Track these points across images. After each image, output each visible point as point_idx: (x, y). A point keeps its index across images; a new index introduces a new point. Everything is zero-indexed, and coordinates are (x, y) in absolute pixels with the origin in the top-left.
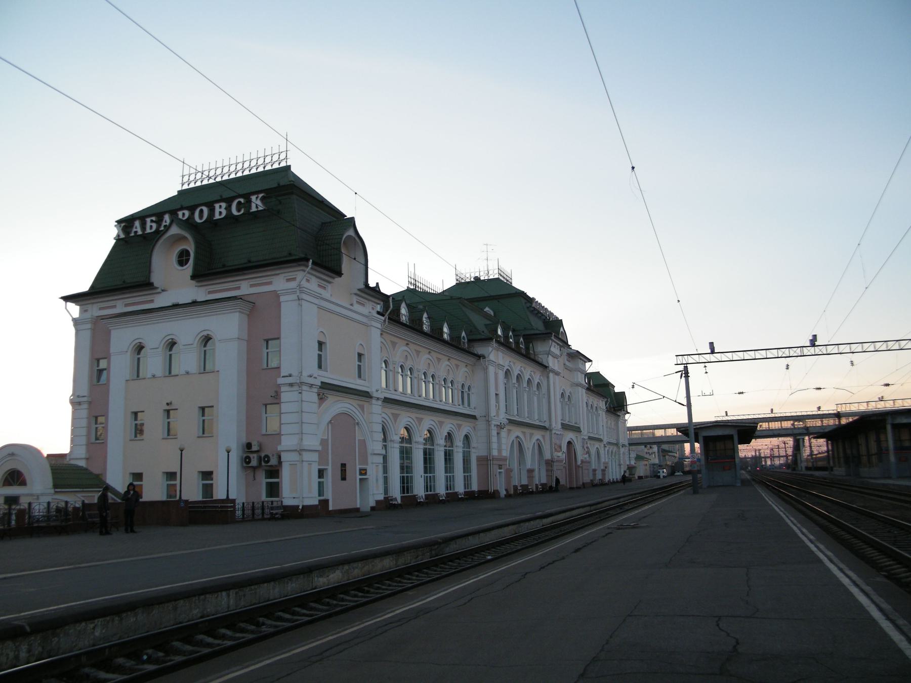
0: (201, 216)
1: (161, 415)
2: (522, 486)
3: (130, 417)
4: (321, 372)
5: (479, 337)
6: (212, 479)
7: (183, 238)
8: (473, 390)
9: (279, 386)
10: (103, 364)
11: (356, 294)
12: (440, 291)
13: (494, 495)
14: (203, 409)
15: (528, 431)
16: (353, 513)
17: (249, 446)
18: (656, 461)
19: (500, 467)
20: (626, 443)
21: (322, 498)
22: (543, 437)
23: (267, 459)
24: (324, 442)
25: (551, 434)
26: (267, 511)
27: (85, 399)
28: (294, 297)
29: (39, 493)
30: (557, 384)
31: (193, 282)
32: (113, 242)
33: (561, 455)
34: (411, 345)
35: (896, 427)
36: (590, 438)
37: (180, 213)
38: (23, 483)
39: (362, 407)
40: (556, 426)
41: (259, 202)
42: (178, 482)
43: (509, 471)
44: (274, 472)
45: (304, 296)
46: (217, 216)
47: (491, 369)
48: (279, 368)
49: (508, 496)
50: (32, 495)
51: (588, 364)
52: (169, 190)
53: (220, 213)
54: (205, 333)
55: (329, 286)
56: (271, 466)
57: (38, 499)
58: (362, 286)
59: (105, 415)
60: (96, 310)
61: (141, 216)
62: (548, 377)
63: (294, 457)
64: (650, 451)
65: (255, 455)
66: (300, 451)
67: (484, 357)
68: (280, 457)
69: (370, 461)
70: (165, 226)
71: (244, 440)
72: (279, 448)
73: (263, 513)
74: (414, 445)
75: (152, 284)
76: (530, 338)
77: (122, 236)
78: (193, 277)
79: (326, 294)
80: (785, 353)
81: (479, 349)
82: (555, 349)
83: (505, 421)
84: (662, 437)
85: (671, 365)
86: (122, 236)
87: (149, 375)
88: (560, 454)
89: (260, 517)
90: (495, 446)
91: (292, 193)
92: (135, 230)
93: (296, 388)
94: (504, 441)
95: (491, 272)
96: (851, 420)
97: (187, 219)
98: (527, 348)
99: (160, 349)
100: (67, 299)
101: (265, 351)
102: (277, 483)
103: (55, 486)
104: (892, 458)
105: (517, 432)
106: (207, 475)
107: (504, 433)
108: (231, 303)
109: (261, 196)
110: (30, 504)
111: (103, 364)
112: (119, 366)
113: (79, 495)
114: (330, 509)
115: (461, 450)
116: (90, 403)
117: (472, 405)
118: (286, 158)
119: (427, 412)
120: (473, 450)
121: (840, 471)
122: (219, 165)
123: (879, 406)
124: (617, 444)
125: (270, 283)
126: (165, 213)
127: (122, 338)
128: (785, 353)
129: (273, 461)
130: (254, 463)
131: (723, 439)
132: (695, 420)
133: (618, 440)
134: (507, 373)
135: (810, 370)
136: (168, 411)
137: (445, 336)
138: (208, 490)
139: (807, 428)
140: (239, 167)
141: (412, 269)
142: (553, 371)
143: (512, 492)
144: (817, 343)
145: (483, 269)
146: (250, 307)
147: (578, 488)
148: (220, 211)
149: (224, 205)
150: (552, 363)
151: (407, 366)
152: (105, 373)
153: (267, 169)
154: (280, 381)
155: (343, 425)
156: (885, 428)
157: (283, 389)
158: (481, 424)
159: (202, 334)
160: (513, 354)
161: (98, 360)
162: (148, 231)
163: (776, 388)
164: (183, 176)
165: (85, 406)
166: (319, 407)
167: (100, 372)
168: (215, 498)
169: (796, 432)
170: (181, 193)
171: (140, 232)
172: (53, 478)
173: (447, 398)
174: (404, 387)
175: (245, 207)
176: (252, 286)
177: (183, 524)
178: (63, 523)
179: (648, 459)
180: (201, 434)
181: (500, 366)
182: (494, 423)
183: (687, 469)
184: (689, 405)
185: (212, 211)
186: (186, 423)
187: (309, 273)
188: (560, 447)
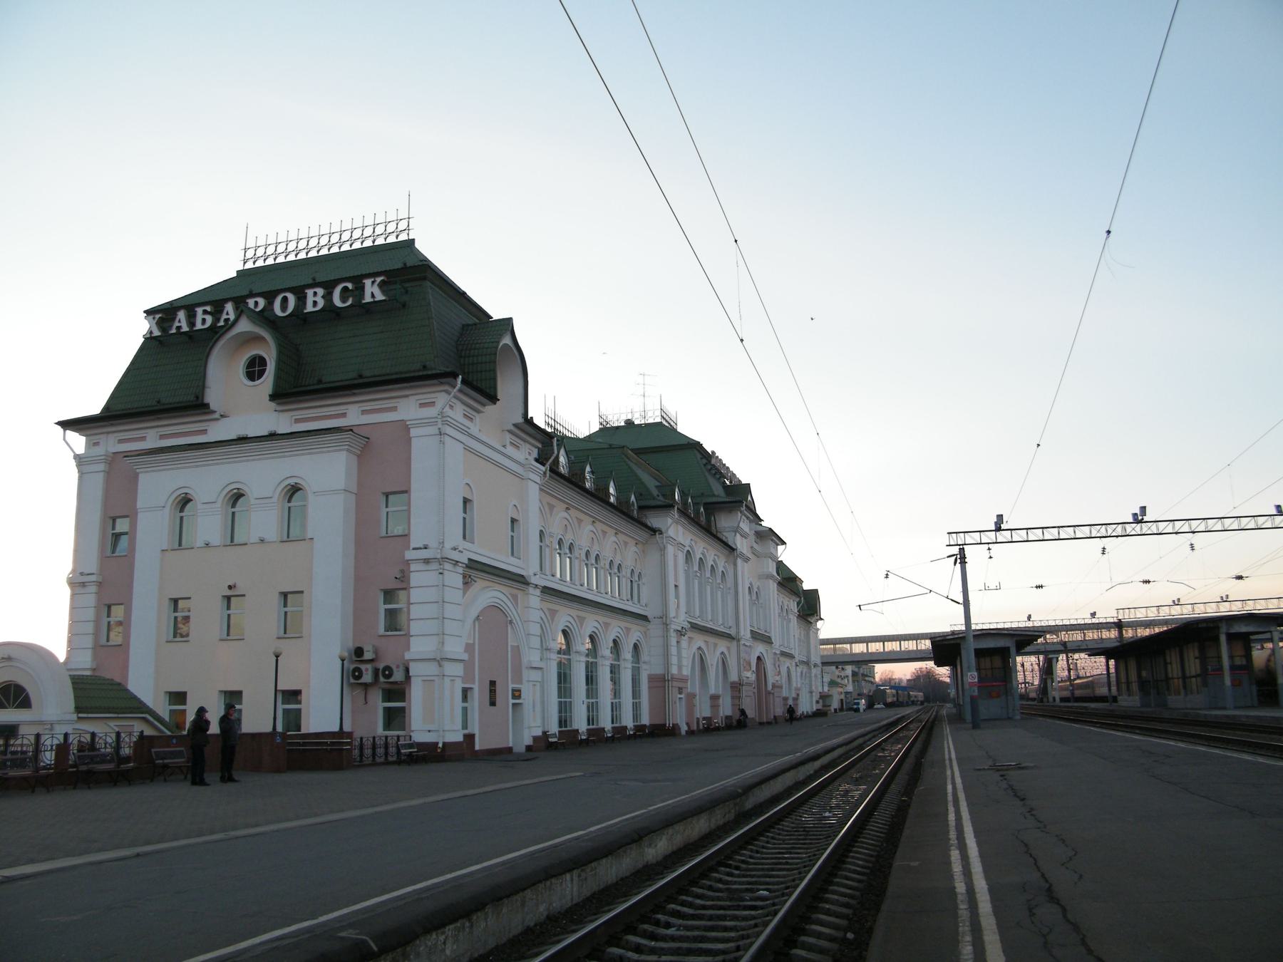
0: (284, 308)
1: (219, 604)
2: (704, 719)
3: (167, 606)
4: (467, 545)
5: (653, 503)
6: (300, 703)
7: (257, 339)
8: (644, 580)
9: (408, 563)
10: (122, 526)
11: (510, 431)
12: (581, 436)
13: (672, 732)
14: (285, 595)
15: (712, 640)
16: (503, 754)
17: (359, 652)
18: (850, 688)
19: (680, 690)
20: (819, 661)
21: (466, 732)
22: (728, 648)
23: (388, 671)
24: (469, 648)
25: (738, 646)
26: (392, 750)
27: (93, 578)
28: (433, 430)
29: (51, 718)
30: (746, 573)
31: (273, 405)
33: (750, 676)
34: (572, 511)
35: (1231, 637)
36: (784, 654)
37: (251, 302)
39: (515, 597)
40: (745, 634)
42: (280, 707)
43: (691, 696)
44: (397, 692)
45: (449, 430)
46: (310, 308)
47: (670, 550)
48: (406, 536)
49: (691, 733)
50: (41, 723)
51: (781, 548)
52: (227, 271)
53: (315, 303)
54: (292, 481)
55: (478, 417)
56: (396, 683)
57: (51, 729)
58: (520, 420)
59: (127, 604)
60: (112, 442)
61: (188, 304)
62: (735, 565)
63: (432, 669)
64: (843, 674)
65: (369, 666)
66: (440, 661)
67: (661, 533)
68: (407, 670)
69: (525, 678)
70: (227, 320)
71: (351, 645)
72: (407, 656)
73: (386, 754)
74: (574, 657)
75: (207, 406)
76: (713, 508)
77: (157, 333)
78: (274, 397)
79: (474, 430)
80: (1104, 531)
81: (655, 521)
82: (745, 526)
83: (687, 625)
84: (862, 653)
85: (942, 548)
86: (157, 333)
87: (200, 543)
88: (749, 674)
89: (382, 760)
90: (674, 660)
91: (425, 278)
92: (177, 324)
93: (434, 566)
94: (684, 653)
95: (650, 414)
96: (1157, 630)
97: (262, 311)
98: (708, 521)
99: (219, 505)
100: (66, 425)
101: (384, 510)
102: (403, 709)
103: (79, 709)
104: (1228, 681)
105: (700, 641)
107: (684, 643)
108: (329, 437)
109: (379, 279)
110: (38, 736)
111: (122, 526)
112: (152, 528)
113: (112, 724)
115: (630, 666)
116: (100, 584)
117: (643, 602)
119: (590, 609)
121: (1131, 701)
122: (272, 240)
123: (1173, 612)
124: (807, 663)
125: (394, 409)
126: (226, 301)
127: (157, 487)
128: (1104, 531)
129: (398, 676)
130: (367, 678)
131: (980, 657)
132: (973, 627)
133: (808, 657)
134: (688, 555)
135: (1134, 553)
136: (228, 598)
137: (612, 499)
138: (294, 719)
139: (1064, 644)
140: (271, 250)
141: (550, 404)
142: (742, 555)
144: (1146, 519)
145: (638, 408)
146: (363, 444)
147: (769, 723)
148: (315, 300)
149: (320, 291)
150: (741, 544)
151: (568, 539)
152: (124, 540)
153: (278, 261)
154: (410, 555)
155: (494, 623)
156: (1217, 639)
157: (413, 567)
158: (655, 629)
159: (287, 482)
160: (694, 529)
161: (114, 520)
162: (199, 326)
164: (246, 250)
165: (93, 589)
166: (464, 594)
167: (117, 537)
168: (303, 731)
169: (1049, 648)
170: (242, 274)
171: (185, 328)
172: (76, 698)
173: (612, 591)
174: (561, 572)
175: (354, 297)
177: (278, 770)
178: (80, 770)
179: (842, 686)
180: (225, 636)
182: (673, 627)
183: (889, 700)
185: (302, 299)
186: (259, 617)
187: (455, 397)
188: (750, 665)
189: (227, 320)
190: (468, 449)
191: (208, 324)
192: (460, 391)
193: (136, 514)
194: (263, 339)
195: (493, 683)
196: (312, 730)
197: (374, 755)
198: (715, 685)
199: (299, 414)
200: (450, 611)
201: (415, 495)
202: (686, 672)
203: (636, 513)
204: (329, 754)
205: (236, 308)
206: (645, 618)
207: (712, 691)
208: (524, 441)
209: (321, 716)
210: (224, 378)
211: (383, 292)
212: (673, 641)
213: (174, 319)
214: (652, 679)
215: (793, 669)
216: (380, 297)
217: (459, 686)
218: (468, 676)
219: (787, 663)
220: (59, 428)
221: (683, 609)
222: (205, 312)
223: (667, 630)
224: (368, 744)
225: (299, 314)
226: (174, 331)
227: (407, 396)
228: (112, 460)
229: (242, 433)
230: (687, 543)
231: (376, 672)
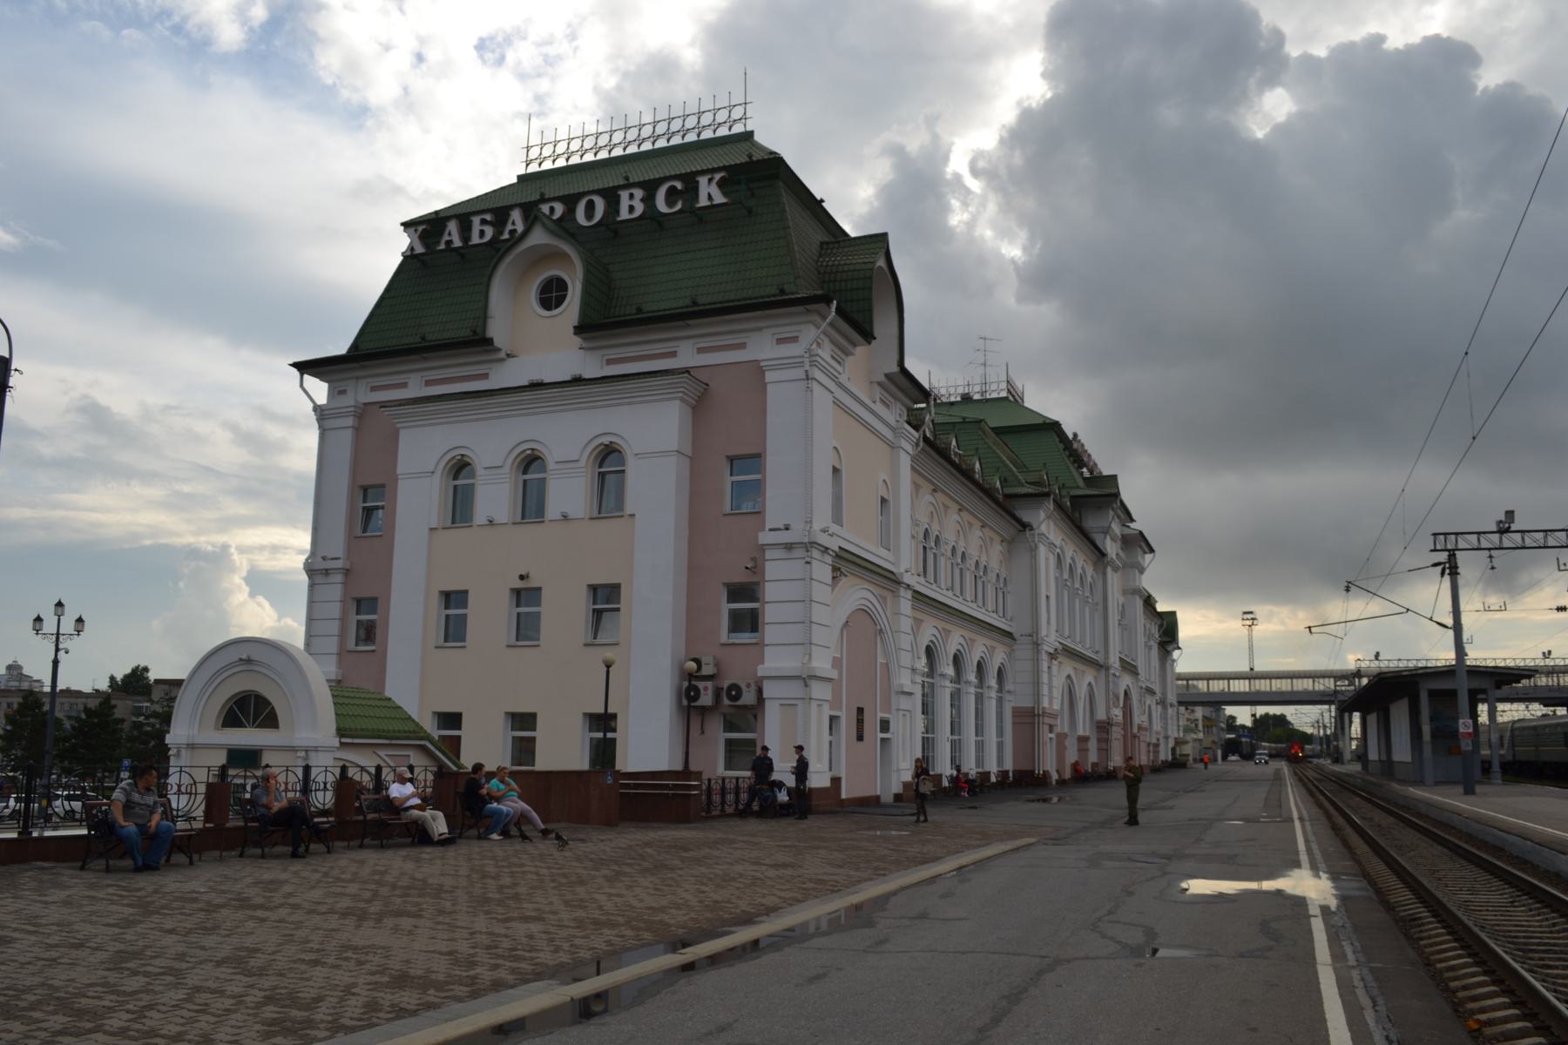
3: (436, 600)
9: (762, 548)
11: (879, 384)
13: (1041, 781)
23: (735, 691)
24: (836, 663)
25: (1107, 676)
27: (339, 564)
28: (800, 373)
31: (578, 340)
32: (398, 260)
33: (1117, 713)
35: (1433, 694)
37: (545, 208)
38: (271, 721)
40: (1114, 661)
41: (715, 191)
45: (818, 374)
46: (624, 214)
47: (1042, 550)
51: (1148, 557)
52: (505, 174)
53: (631, 209)
54: (606, 440)
57: (306, 758)
61: (462, 214)
62: (1105, 574)
63: (793, 690)
65: (709, 684)
66: (806, 679)
68: (760, 691)
70: (513, 232)
72: (762, 671)
75: (490, 341)
77: (420, 249)
78: (579, 330)
82: (1116, 528)
86: (420, 249)
92: (446, 238)
93: (799, 553)
94: (1055, 682)
97: (560, 219)
99: (507, 469)
100: (304, 367)
103: (341, 732)
106: (523, 720)
107: (1055, 669)
109: (718, 176)
112: (417, 501)
114: (843, 796)
116: (347, 572)
117: (1009, 615)
118: (744, 118)
120: (1007, 697)
125: (742, 346)
126: (512, 207)
127: (421, 450)
129: (748, 698)
130: (706, 699)
138: (604, 752)
143: (1068, 774)
146: (701, 396)
148: (631, 205)
149: (639, 193)
150: (1111, 548)
153: (703, 137)
154: (765, 538)
155: (864, 630)
157: (769, 554)
158: (1023, 651)
162: (475, 240)
163: (399, 700)
165: (339, 578)
171: (457, 243)
176: (701, 350)
181: (1052, 545)
184: (1457, 628)
187: (824, 333)
189: (513, 232)
190: (837, 403)
191: (488, 237)
192: (831, 324)
193: (396, 480)
194: (565, 256)
195: (860, 711)
196: (631, 769)
197: (723, 802)
198: (1083, 728)
199: (613, 353)
200: (818, 613)
201: (772, 462)
202: (1056, 706)
203: (1007, 506)
204: (661, 801)
205: (526, 218)
206: (1009, 635)
207: (1081, 732)
208: (896, 399)
209: (648, 746)
210: (511, 310)
211: (725, 194)
212: (1045, 665)
213: (441, 234)
214: (1018, 713)
215: (1153, 707)
216: (719, 199)
217: (827, 711)
218: (835, 702)
219: (1149, 700)
220: (295, 370)
221: (1054, 626)
222: (484, 222)
223: (1038, 651)
224: (716, 786)
225: (610, 226)
226: (442, 246)
227: (760, 329)
228: (363, 413)
229: (536, 376)
230: (1058, 543)
231: (718, 692)
